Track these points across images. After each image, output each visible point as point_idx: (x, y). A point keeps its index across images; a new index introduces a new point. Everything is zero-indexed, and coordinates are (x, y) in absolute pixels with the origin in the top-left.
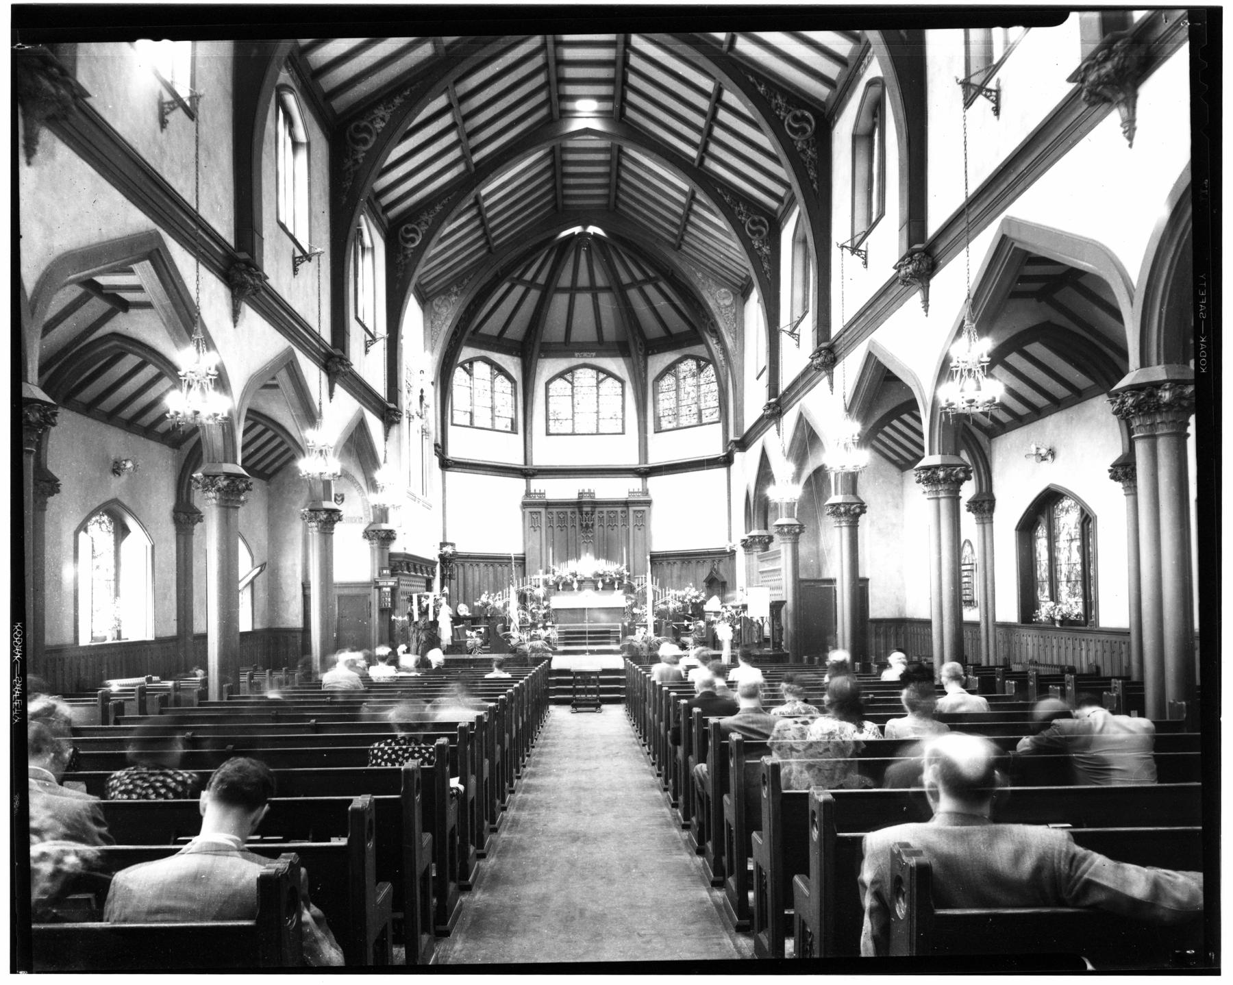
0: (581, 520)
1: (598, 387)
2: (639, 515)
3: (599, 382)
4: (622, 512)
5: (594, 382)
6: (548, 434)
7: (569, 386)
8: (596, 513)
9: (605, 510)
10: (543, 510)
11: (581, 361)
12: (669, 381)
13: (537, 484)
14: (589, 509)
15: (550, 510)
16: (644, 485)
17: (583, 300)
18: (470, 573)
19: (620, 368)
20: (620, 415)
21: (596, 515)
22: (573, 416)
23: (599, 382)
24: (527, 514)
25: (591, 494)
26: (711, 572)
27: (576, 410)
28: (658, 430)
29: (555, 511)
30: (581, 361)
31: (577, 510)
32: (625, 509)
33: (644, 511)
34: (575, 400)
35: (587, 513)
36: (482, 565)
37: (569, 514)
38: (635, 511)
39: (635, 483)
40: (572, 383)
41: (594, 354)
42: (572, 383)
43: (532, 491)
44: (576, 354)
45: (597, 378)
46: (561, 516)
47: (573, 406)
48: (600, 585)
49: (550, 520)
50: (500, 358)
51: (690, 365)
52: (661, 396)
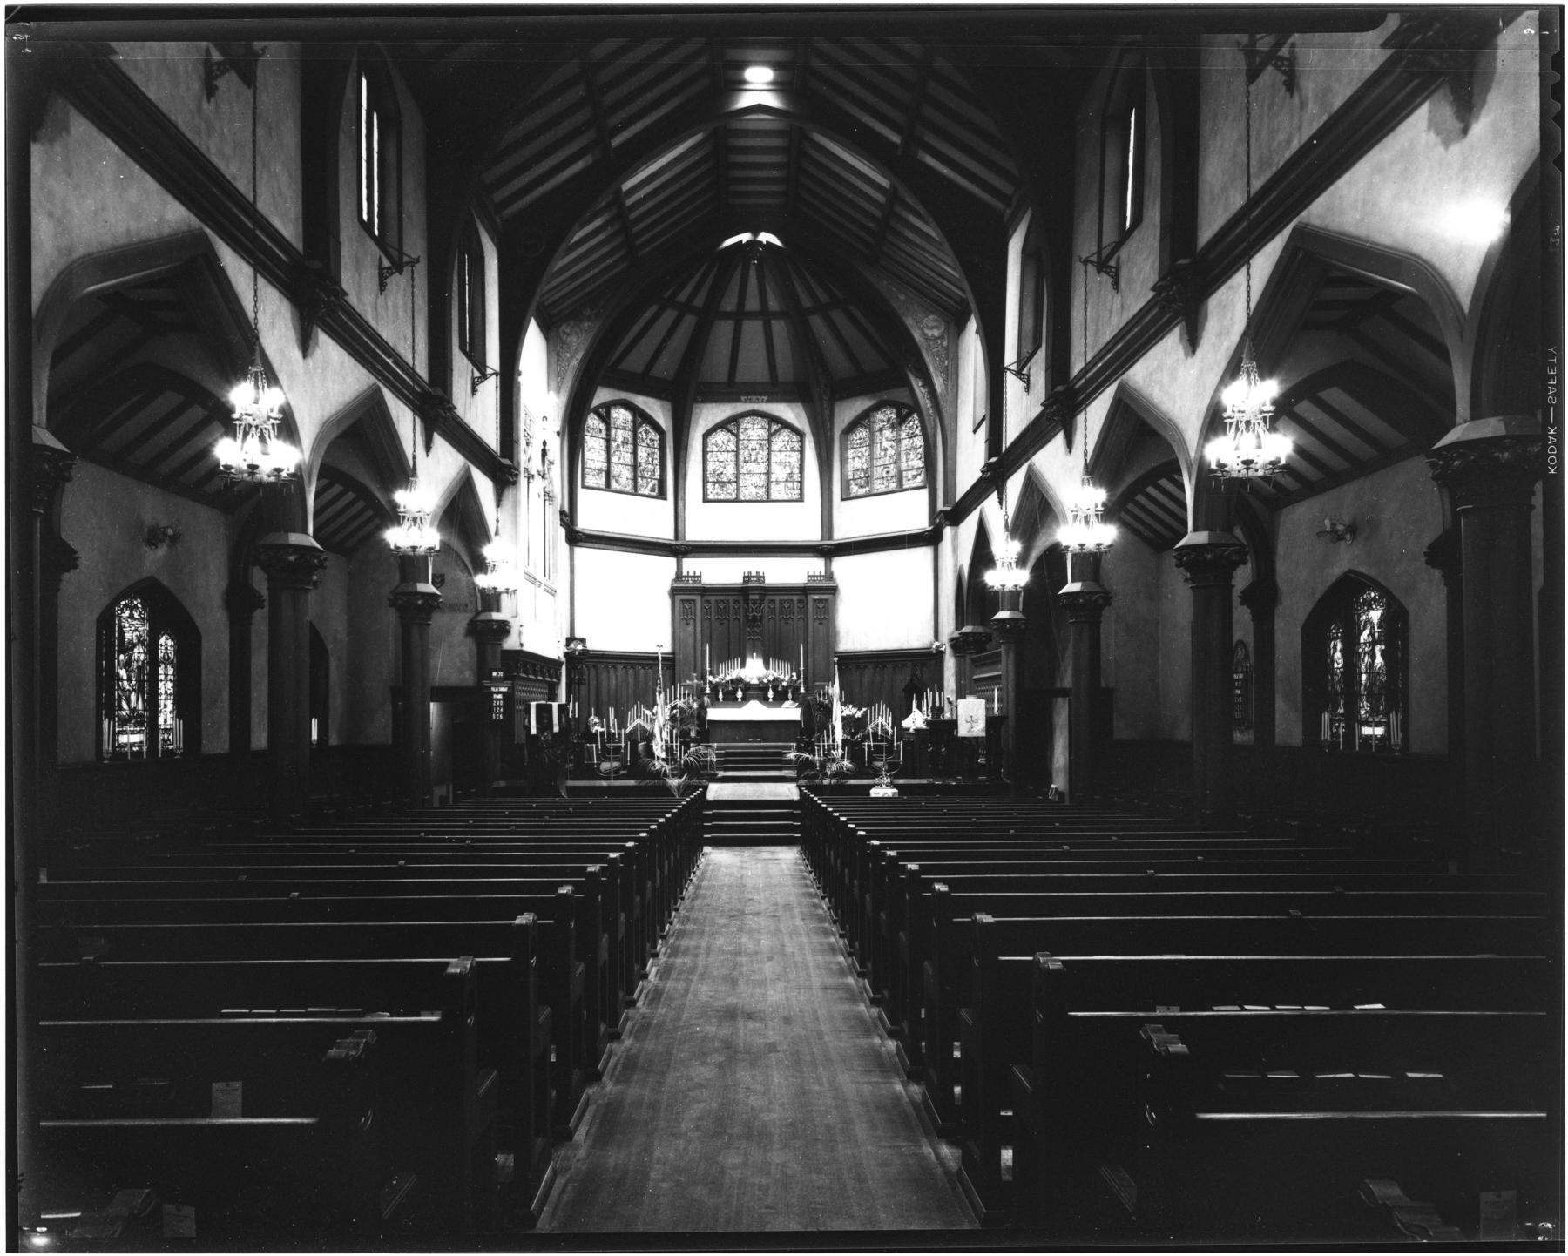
0: (746, 611)
1: (770, 442)
2: (821, 606)
3: (771, 435)
4: (799, 601)
5: (764, 433)
6: (706, 500)
7: (733, 438)
8: (766, 602)
9: (777, 598)
10: (698, 598)
11: (748, 407)
12: (861, 434)
13: (691, 565)
14: (757, 597)
15: (706, 598)
16: (828, 566)
17: (753, 329)
18: (604, 676)
19: (797, 416)
20: (797, 477)
21: (766, 606)
22: (737, 477)
23: (771, 435)
24: (677, 605)
25: (760, 578)
26: (912, 680)
27: (741, 471)
28: (846, 497)
29: (713, 599)
30: (748, 407)
31: (741, 598)
32: (803, 597)
33: (826, 600)
34: (741, 458)
35: (754, 602)
36: (620, 667)
37: (732, 604)
38: (815, 600)
39: (816, 565)
40: (736, 435)
41: (765, 398)
42: (736, 435)
43: (685, 573)
44: (743, 398)
45: (769, 430)
46: (721, 606)
47: (737, 465)
48: (771, 694)
49: (706, 612)
50: (645, 403)
51: (890, 414)
52: (851, 453)
